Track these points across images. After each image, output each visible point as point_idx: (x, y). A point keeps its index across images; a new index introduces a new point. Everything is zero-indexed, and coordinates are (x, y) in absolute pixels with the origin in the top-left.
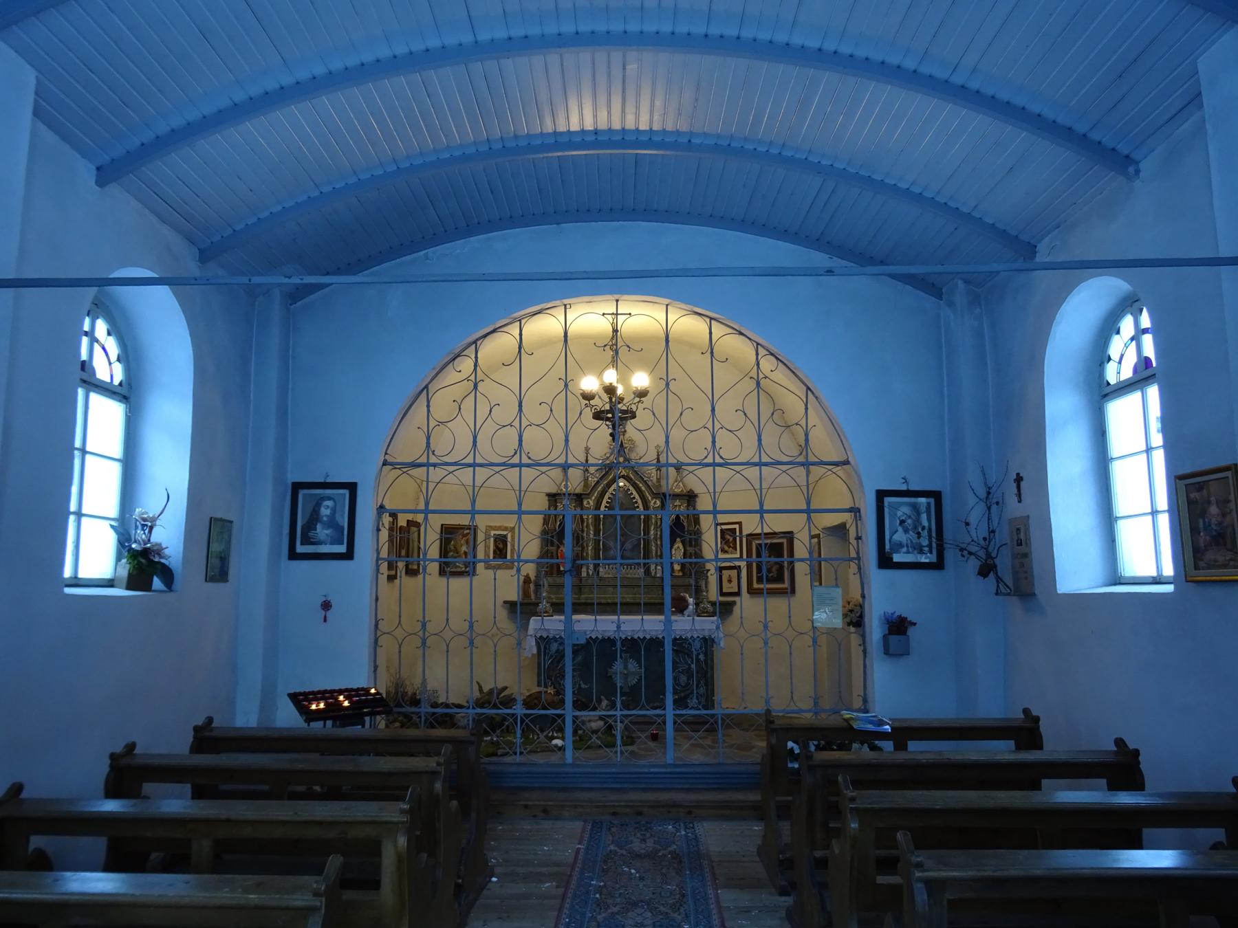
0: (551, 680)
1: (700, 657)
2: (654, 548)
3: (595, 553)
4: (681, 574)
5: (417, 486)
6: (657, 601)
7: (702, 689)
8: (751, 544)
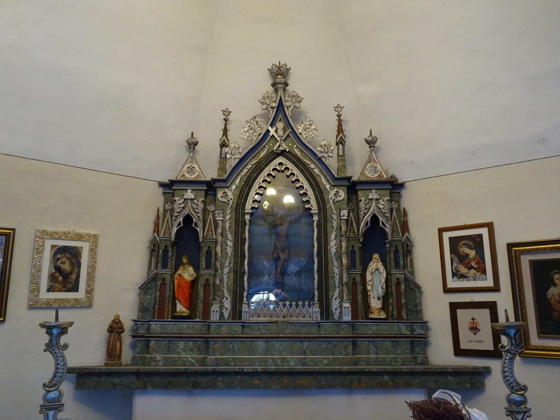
2: (336, 271)
3: (235, 280)
4: (383, 315)
6: (345, 368)
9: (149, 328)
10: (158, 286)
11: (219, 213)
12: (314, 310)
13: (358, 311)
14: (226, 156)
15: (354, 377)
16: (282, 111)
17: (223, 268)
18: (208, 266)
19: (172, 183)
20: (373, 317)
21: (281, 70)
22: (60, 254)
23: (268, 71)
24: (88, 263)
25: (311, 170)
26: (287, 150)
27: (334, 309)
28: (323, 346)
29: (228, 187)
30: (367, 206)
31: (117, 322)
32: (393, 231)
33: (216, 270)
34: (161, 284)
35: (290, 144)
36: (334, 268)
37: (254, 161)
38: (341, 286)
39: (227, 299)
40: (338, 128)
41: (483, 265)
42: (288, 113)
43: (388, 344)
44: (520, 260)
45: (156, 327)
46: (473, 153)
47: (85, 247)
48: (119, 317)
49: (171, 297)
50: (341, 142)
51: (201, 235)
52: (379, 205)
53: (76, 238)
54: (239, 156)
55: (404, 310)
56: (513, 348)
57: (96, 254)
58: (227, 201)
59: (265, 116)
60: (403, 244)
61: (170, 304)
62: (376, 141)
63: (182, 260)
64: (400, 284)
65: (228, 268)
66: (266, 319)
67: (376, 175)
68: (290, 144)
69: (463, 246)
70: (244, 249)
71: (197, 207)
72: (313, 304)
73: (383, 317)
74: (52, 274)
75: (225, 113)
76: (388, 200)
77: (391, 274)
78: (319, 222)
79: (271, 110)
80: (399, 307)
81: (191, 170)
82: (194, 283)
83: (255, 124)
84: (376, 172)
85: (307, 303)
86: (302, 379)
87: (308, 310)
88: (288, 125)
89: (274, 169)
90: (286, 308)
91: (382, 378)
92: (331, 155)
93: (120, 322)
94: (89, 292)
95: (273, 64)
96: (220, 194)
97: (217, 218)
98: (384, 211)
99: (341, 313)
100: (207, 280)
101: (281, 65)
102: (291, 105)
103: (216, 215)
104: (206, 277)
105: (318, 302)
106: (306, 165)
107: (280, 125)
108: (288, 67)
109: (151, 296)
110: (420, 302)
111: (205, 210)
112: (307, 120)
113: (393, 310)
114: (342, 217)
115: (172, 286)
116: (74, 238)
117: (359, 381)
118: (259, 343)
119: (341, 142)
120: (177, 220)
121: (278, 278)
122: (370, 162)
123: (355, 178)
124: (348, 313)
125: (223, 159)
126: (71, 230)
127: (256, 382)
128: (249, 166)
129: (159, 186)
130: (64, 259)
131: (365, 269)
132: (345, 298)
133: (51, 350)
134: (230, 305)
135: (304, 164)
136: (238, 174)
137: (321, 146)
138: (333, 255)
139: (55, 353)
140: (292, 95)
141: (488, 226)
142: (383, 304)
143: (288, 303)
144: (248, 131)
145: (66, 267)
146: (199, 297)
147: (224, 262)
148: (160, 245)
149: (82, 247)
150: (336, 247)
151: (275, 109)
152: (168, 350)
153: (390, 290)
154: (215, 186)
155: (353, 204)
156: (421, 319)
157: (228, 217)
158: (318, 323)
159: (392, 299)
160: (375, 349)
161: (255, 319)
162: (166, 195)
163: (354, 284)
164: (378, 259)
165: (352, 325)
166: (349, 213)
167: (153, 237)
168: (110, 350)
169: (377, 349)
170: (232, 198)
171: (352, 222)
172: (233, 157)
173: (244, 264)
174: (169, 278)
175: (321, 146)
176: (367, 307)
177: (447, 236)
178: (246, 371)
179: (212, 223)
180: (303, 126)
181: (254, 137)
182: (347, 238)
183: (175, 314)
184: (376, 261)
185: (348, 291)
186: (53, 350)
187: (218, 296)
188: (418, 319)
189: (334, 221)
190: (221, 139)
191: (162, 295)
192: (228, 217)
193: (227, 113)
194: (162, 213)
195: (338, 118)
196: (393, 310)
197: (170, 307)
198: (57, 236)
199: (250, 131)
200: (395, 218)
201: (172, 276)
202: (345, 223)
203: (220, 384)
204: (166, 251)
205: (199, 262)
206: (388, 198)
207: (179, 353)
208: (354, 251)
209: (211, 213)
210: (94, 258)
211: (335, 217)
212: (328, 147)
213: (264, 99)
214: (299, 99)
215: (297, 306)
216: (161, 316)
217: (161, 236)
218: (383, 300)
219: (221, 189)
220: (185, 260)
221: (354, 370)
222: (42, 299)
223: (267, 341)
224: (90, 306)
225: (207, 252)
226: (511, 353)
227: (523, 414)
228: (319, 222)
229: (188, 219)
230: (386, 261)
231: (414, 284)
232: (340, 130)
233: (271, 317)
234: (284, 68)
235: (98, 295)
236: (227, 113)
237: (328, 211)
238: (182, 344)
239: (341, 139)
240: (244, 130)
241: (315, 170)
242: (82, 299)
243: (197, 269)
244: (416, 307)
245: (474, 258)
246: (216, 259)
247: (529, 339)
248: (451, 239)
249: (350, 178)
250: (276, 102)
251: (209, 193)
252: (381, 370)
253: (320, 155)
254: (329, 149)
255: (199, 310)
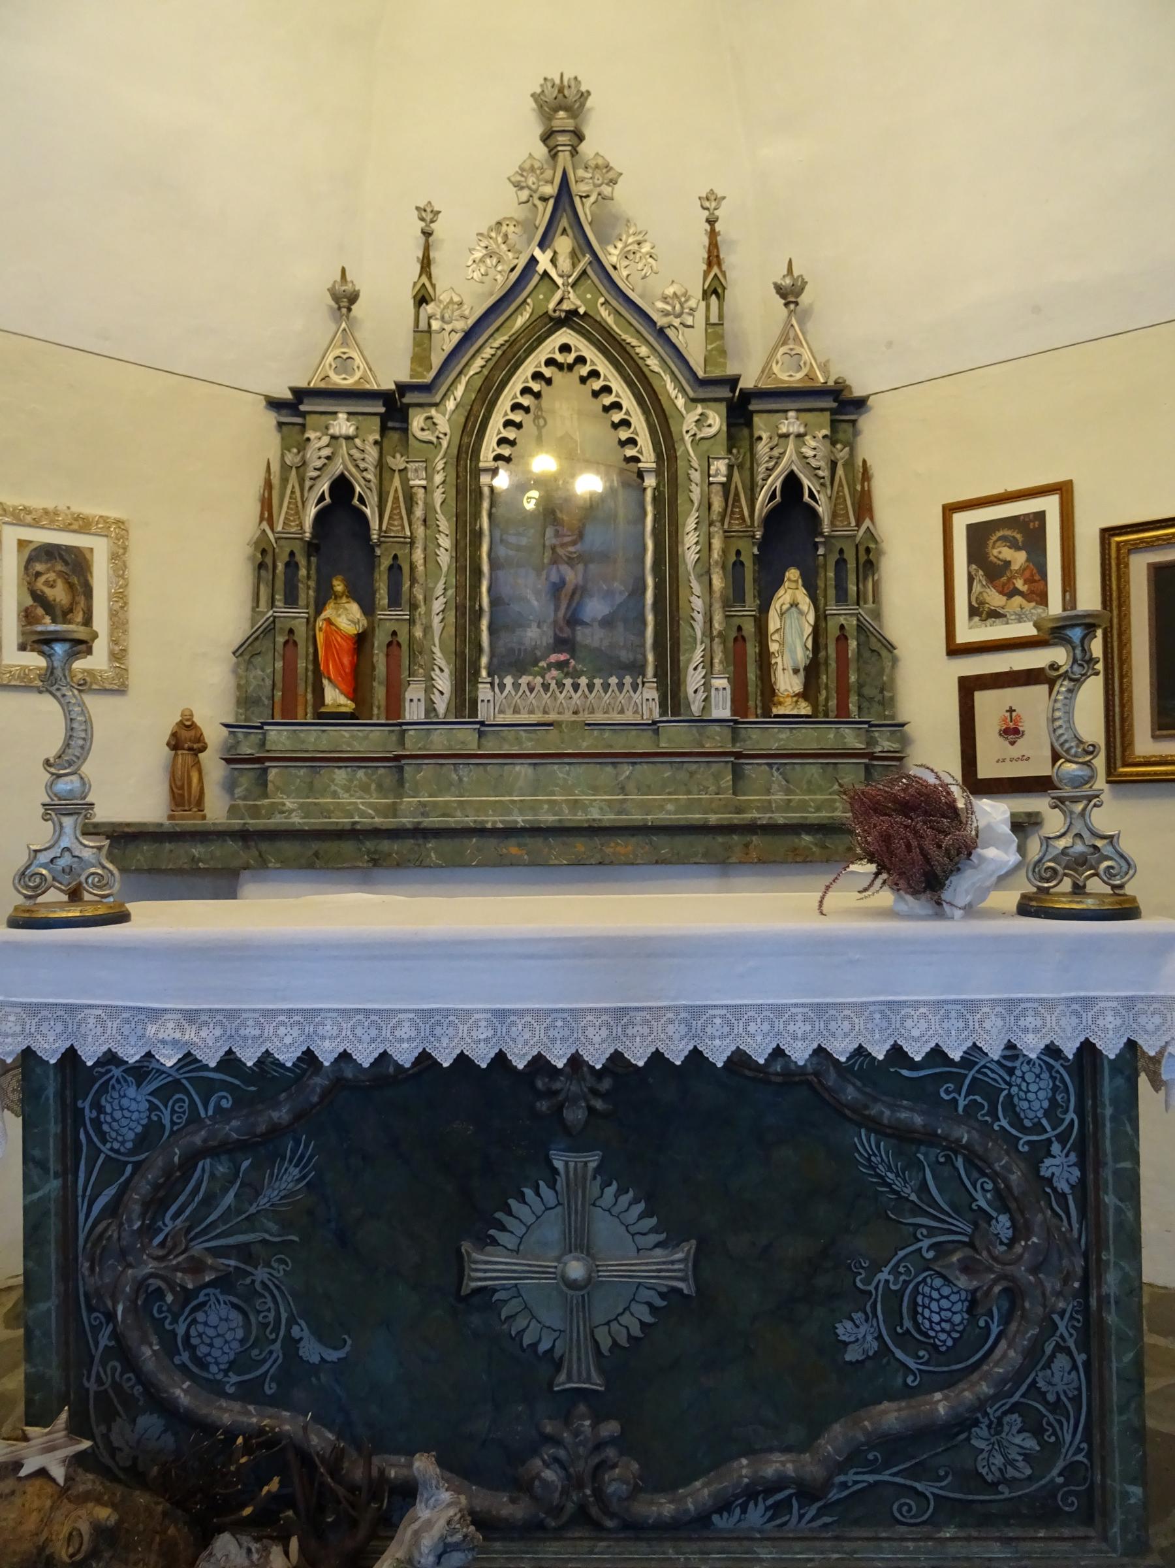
0: (110, 1316)
1: (1048, 1167)
2: (698, 604)
3: (459, 629)
4: (804, 709)
5: (830, 894)
6: (713, 819)
7: (1062, 1361)
8: (1123, 565)
9: (263, 744)
10: (279, 647)
11: (416, 470)
12: (646, 696)
13: (747, 701)
14: (429, 325)
15: (735, 837)
16: (568, 209)
17: (431, 600)
18: (395, 601)
19: (300, 394)
20: (781, 712)
21: (565, 97)
22: (40, 561)
23: (531, 99)
24: (109, 589)
25: (640, 362)
26: (582, 311)
27: (690, 691)
28: (666, 775)
29: (436, 405)
30: (776, 453)
31: (188, 727)
32: (834, 515)
33: (414, 607)
34: (286, 643)
35: (589, 296)
36: (693, 599)
37: (500, 340)
38: (707, 641)
39: (442, 670)
40: (709, 252)
41: (1041, 585)
42: (585, 211)
43: (813, 771)
44: (1127, 566)
45: (279, 738)
46: (1037, 310)
47: (99, 550)
48: (192, 715)
49: (310, 674)
50: (715, 290)
51: (374, 525)
52: (803, 450)
53: (75, 527)
54: (462, 325)
55: (854, 698)
56: (1076, 668)
57: (126, 567)
58: (434, 440)
59: (527, 226)
60: (857, 546)
61: (309, 690)
62: (803, 289)
63: (332, 587)
64: (846, 638)
65: (442, 600)
66: (534, 718)
67: (799, 375)
68: (589, 296)
69: (998, 543)
70: (480, 557)
71: (362, 456)
72: (643, 683)
73: (803, 712)
74: (26, 610)
75: (424, 214)
76: (825, 437)
77: (826, 616)
78: (659, 492)
79: (540, 204)
80: (843, 691)
81: (344, 363)
82: (361, 641)
83: (500, 240)
84: (799, 368)
85: (628, 680)
86: (618, 844)
87: (631, 698)
88: (584, 245)
89: (550, 362)
90: (580, 692)
91: (796, 840)
92: (689, 321)
93: (192, 726)
94: (118, 656)
95: (545, 79)
96: (417, 422)
97: (412, 483)
98: (814, 463)
99: (707, 699)
100: (394, 633)
101: (566, 83)
102: (591, 191)
103: (410, 475)
104: (390, 626)
105: (655, 676)
106: (628, 348)
107: (563, 244)
108: (583, 89)
109: (263, 670)
110: (892, 680)
111: (381, 465)
112: (631, 232)
113: (827, 700)
114: (715, 476)
115: (311, 650)
116: (70, 524)
117: (747, 846)
118: (518, 768)
119: (715, 290)
120: (315, 489)
121: (561, 630)
122: (784, 343)
123: (748, 382)
124: (724, 702)
125: (423, 335)
126: (62, 507)
127: (514, 850)
128: (488, 352)
129: (266, 408)
130: (51, 576)
131: (764, 608)
132: (717, 667)
133: (53, 689)
134: (448, 683)
135: (622, 347)
136: (461, 373)
137: (665, 299)
138: (690, 567)
139: (64, 696)
140: (592, 163)
141: (1060, 489)
142: (807, 685)
143: (583, 681)
144: (482, 260)
145: (58, 594)
146: (376, 673)
147: (431, 585)
148: (277, 550)
149: (91, 550)
150: (698, 548)
151: (551, 202)
152: (311, 789)
153: (822, 654)
154: (406, 400)
155: (742, 451)
156: (893, 717)
157: (438, 479)
158: (654, 723)
159: (827, 674)
160: (784, 783)
161: (509, 718)
162: (285, 428)
163: (740, 639)
164: (796, 581)
165: (734, 725)
166: (730, 467)
167: (259, 532)
168: (179, 789)
169: (787, 781)
170: (448, 431)
171: (737, 494)
172: (448, 328)
173: (480, 593)
174: (304, 629)
175: (665, 299)
176: (768, 692)
177: (961, 521)
178: (489, 825)
179: (401, 499)
180: (620, 245)
181: (499, 277)
182: (725, 532)
183: (323, 710)
184: (793, 585)
185: (725, 651)
186: (58, 689)
187: (421, 666)
188: (885, 717)
189: (693, 487)
190: (415, 284)
191: (290, 669)
192: (438, 479)
193: (428, 215)
194: (278, 474)
195: (708, 227)
196: (827, 700)
197: (310, 696)
198: (29, 518)
199: (488, 261)
200: (841, 485)
201: (310, 623)
202: (721, 493)
203: (433, 855)
204: (292, 565)
205: (373, 593)
206: (826, 432)
207: (335, 795)
208: (742, 564)
209: (397, 474)
210: (122, 576)
211: (696, 476)
212: (683, 299)
213: (522, 175)
214: (611, 175)
215: (606, 687)
216: (288, 712)
217: (279, 528)
218: (806, 678)
219: (419, 409)
220: (339, 586)
221: (736, 822)
222: (9, 666)
223: (535, 764)
224: (121, 690)
225: (391, 568)
226: (1071, 680)
227: (1085, 802)
228: (659, 492)
229: (342, 487)
230: (816, 587)
231: (879, 641)
232: (713, 258)
233: (545, 712)
234: (574, 90)
235: (139, 664)
236: (428, 215)
237: (681, 463)
238: (341, 775)
239: (716, 283)
240: (472, 257)
241: (649, 362)
242: (101, 671)
243: (368, 609)
244: (882, 691)
245: (1022, 570)
246: (413, 580)
247: (1131, 743)
248: (972, 529)
249: (733, 381)
250: (552, 183)
251: (390, 424)
252: (795, 821)
253: (661, 321)
254: (686, 306)
255: (376, 703)
